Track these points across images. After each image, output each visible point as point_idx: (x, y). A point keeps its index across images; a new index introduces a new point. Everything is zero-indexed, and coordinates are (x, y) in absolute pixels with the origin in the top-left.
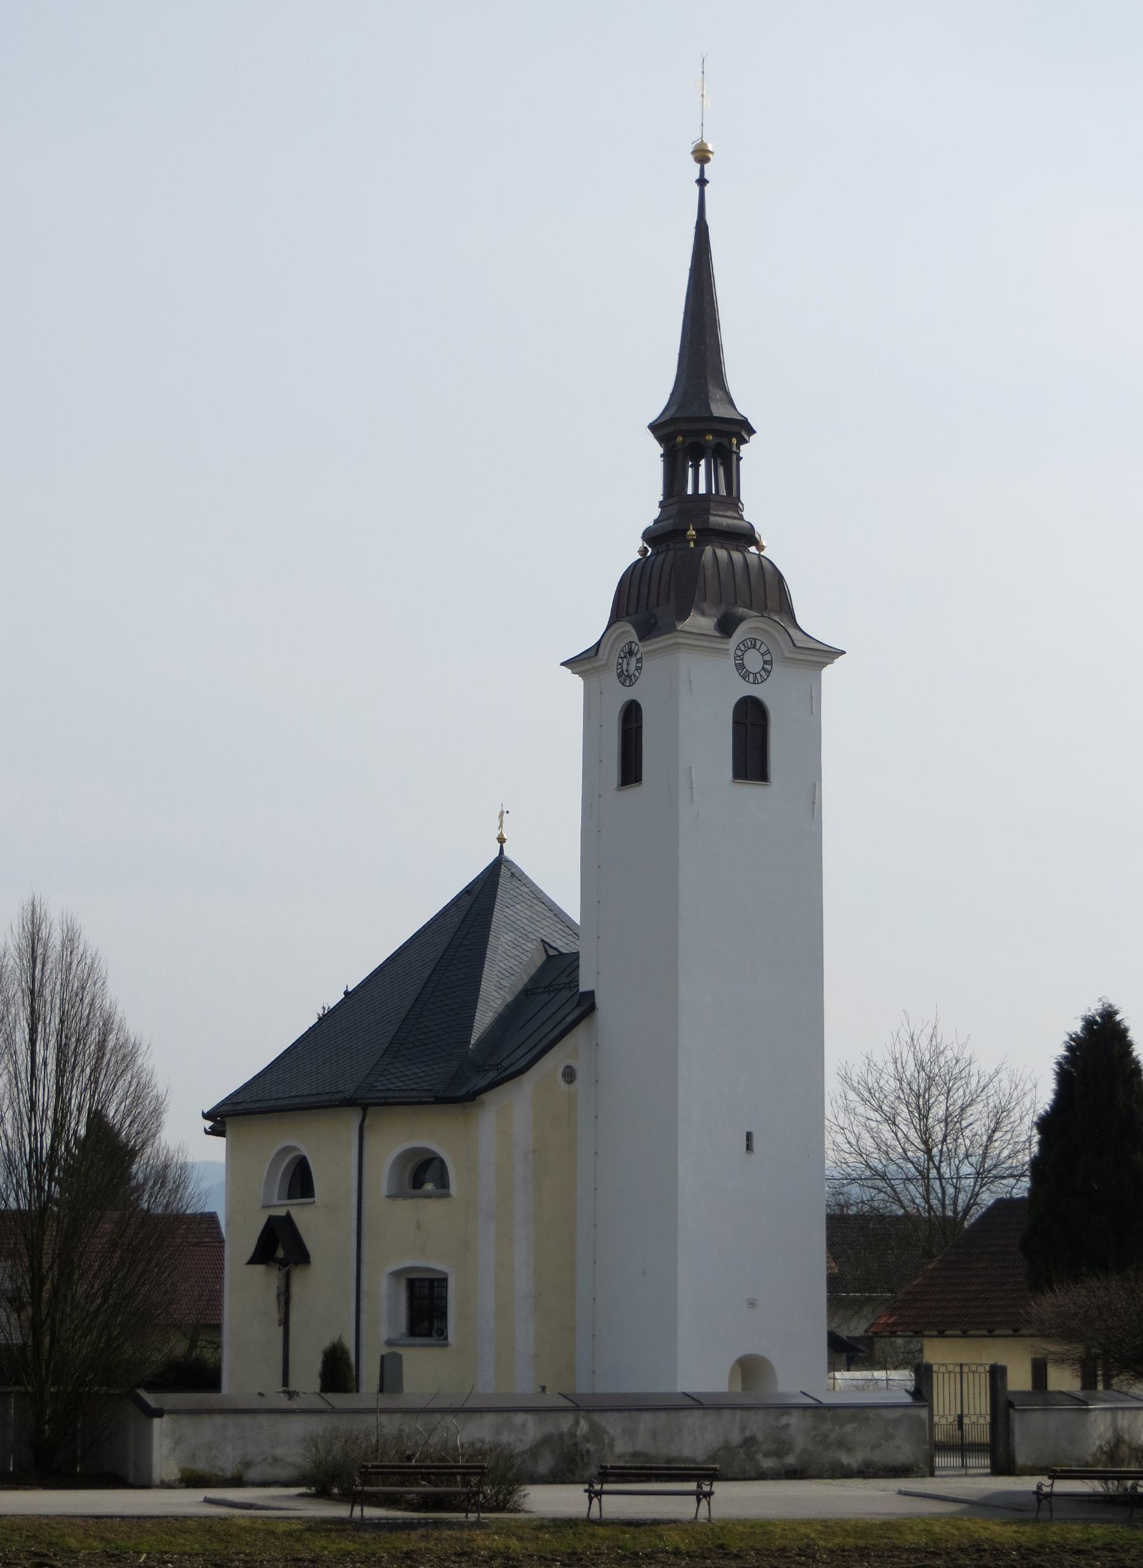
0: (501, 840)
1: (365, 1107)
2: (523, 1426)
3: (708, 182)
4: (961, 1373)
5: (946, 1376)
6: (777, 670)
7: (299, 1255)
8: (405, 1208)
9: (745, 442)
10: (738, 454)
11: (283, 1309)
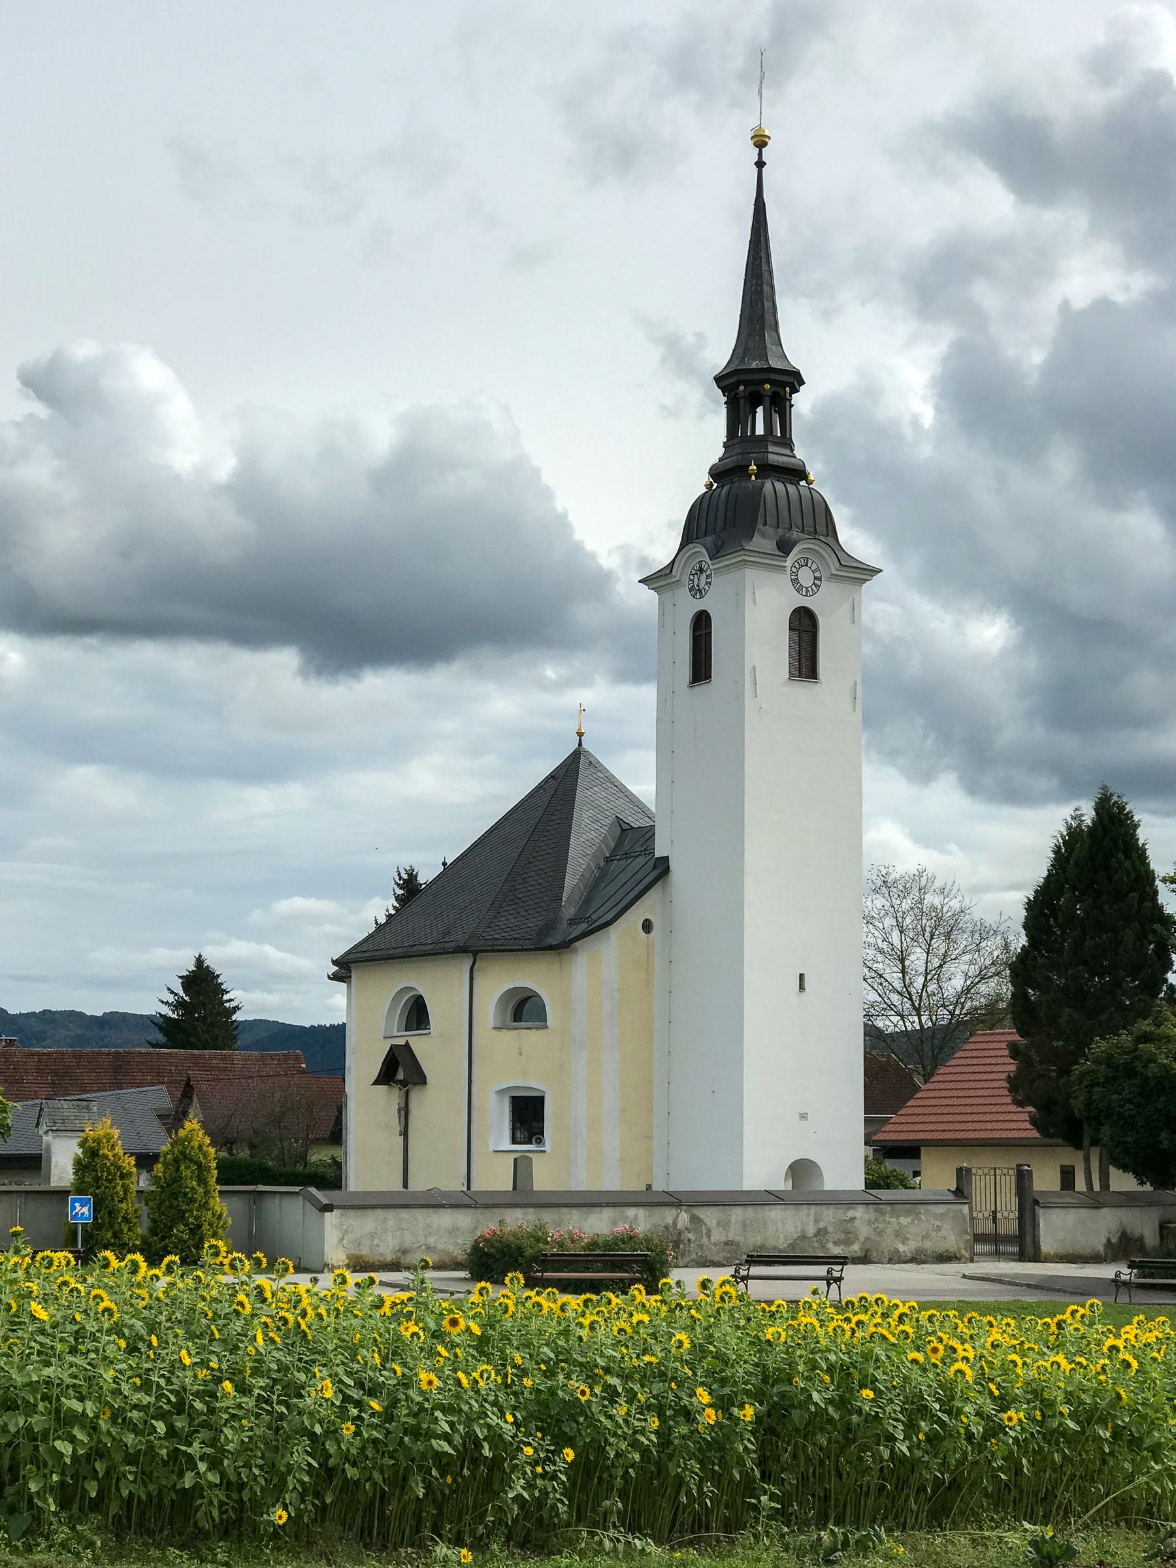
0: (580, 734)
1: (475, 954)
2: (636, 1218)
3: (765, 164)
4: (995, 1175)
5: (983, 1177)
6: (825, 585)
7: (418, 1077)
8: (510, 1039)
9: (797, 391)
10: (790, 401)
11: (403, 1122)
